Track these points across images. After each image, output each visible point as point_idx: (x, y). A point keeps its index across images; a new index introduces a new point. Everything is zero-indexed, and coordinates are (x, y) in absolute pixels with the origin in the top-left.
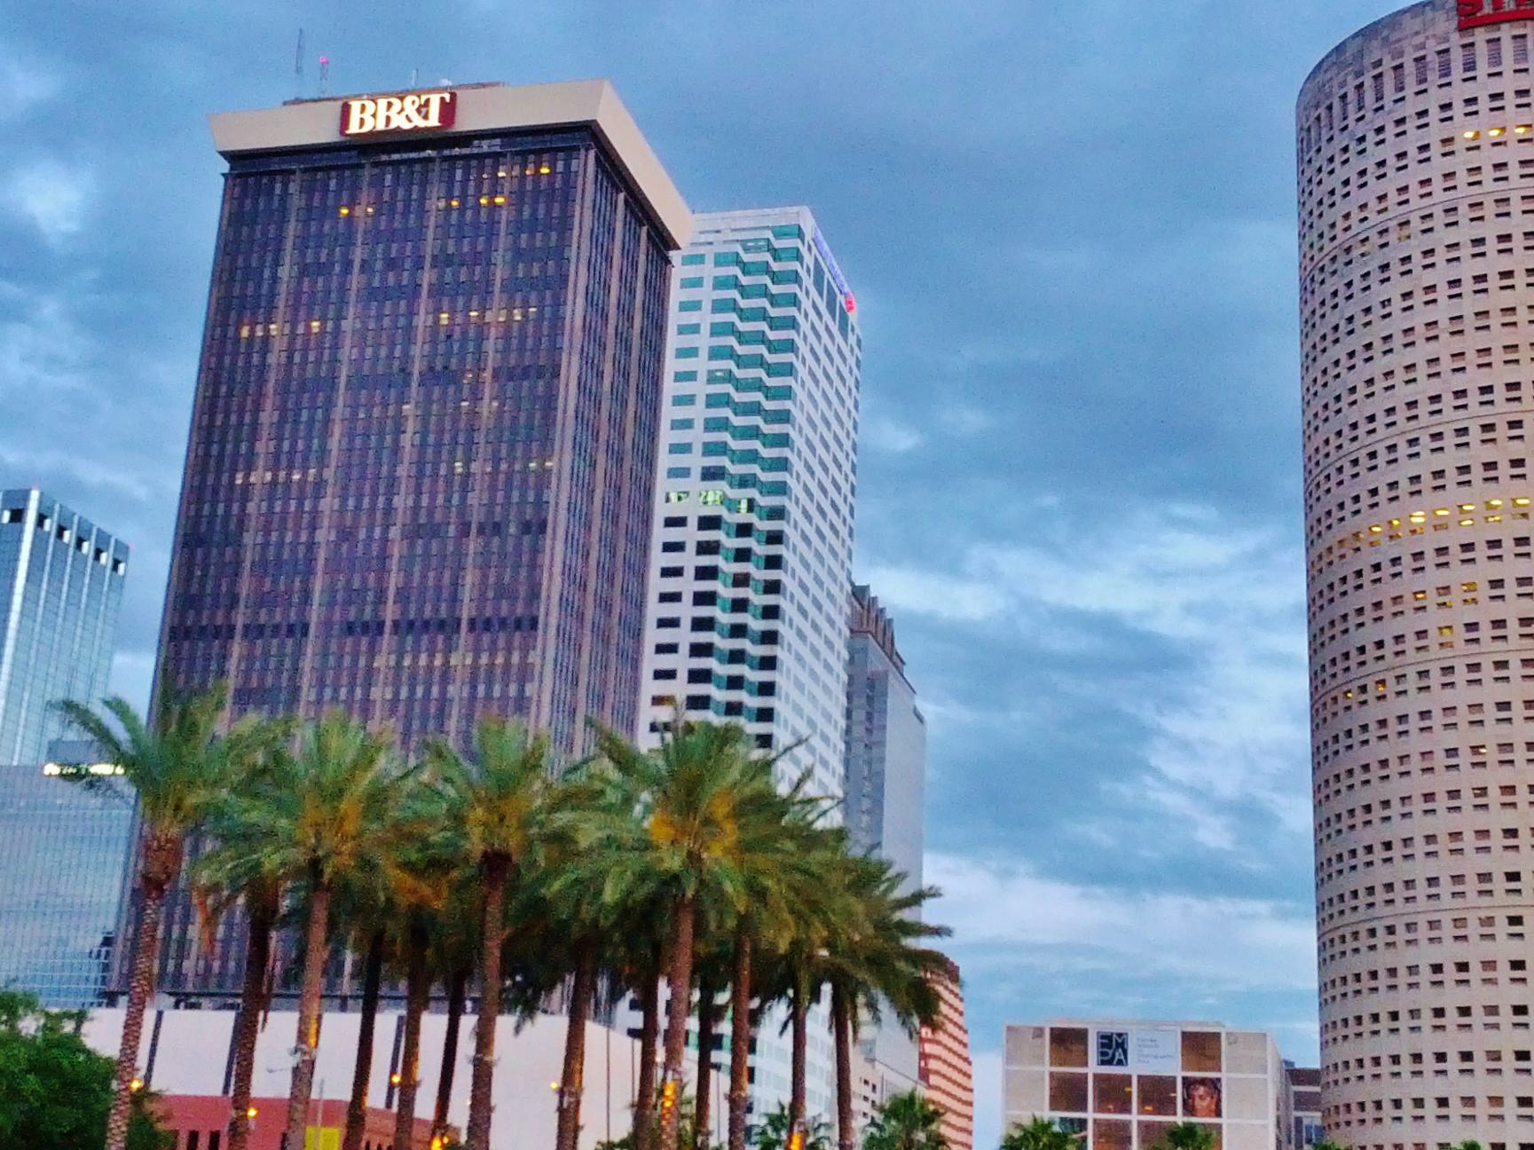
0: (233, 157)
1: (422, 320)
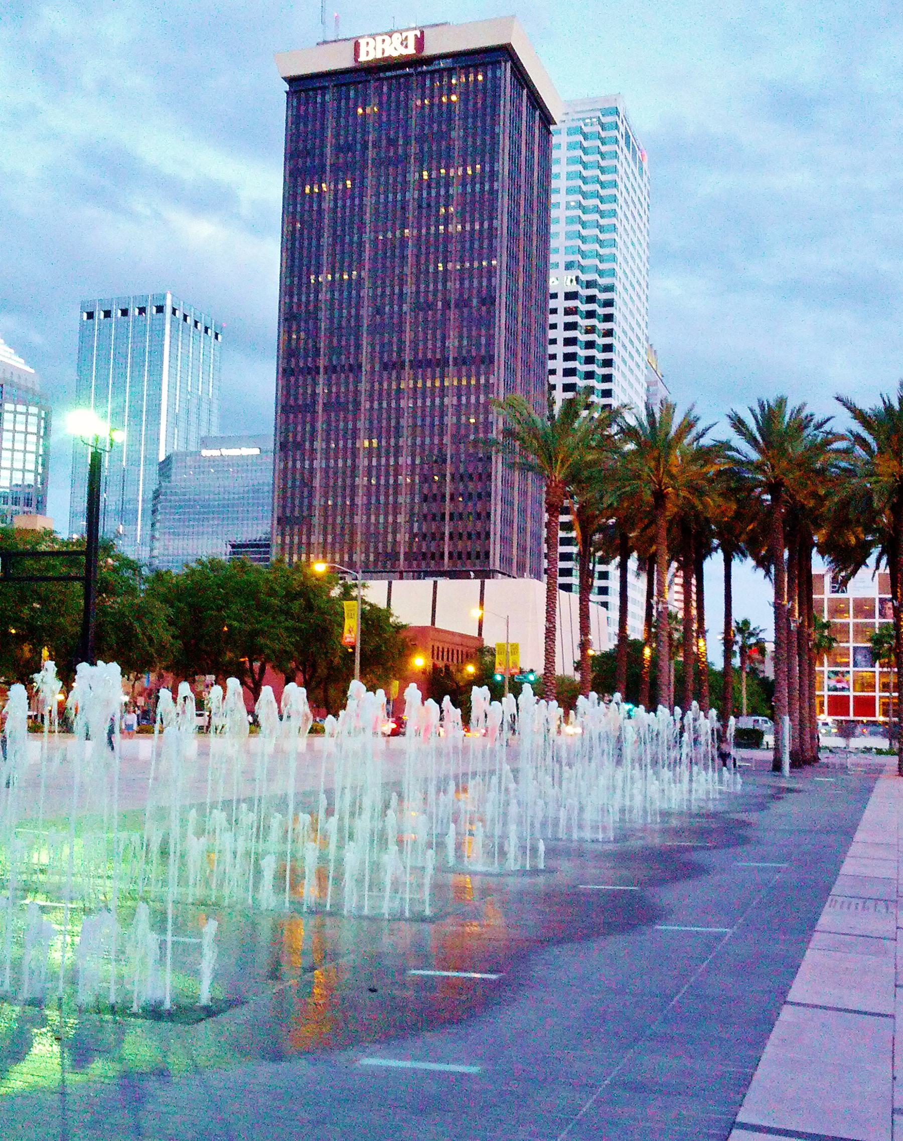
0: (291, 80)
1: (413, 177)
